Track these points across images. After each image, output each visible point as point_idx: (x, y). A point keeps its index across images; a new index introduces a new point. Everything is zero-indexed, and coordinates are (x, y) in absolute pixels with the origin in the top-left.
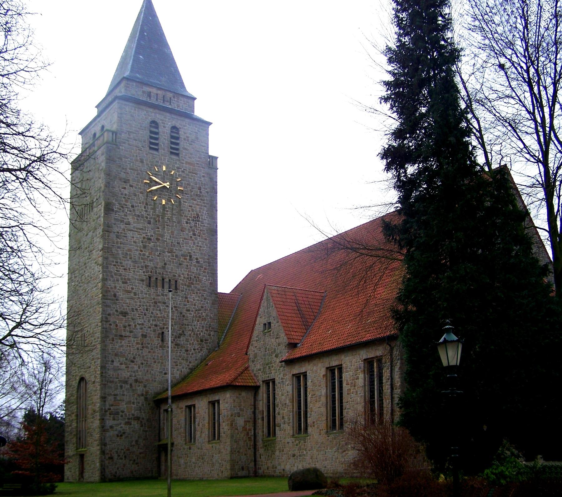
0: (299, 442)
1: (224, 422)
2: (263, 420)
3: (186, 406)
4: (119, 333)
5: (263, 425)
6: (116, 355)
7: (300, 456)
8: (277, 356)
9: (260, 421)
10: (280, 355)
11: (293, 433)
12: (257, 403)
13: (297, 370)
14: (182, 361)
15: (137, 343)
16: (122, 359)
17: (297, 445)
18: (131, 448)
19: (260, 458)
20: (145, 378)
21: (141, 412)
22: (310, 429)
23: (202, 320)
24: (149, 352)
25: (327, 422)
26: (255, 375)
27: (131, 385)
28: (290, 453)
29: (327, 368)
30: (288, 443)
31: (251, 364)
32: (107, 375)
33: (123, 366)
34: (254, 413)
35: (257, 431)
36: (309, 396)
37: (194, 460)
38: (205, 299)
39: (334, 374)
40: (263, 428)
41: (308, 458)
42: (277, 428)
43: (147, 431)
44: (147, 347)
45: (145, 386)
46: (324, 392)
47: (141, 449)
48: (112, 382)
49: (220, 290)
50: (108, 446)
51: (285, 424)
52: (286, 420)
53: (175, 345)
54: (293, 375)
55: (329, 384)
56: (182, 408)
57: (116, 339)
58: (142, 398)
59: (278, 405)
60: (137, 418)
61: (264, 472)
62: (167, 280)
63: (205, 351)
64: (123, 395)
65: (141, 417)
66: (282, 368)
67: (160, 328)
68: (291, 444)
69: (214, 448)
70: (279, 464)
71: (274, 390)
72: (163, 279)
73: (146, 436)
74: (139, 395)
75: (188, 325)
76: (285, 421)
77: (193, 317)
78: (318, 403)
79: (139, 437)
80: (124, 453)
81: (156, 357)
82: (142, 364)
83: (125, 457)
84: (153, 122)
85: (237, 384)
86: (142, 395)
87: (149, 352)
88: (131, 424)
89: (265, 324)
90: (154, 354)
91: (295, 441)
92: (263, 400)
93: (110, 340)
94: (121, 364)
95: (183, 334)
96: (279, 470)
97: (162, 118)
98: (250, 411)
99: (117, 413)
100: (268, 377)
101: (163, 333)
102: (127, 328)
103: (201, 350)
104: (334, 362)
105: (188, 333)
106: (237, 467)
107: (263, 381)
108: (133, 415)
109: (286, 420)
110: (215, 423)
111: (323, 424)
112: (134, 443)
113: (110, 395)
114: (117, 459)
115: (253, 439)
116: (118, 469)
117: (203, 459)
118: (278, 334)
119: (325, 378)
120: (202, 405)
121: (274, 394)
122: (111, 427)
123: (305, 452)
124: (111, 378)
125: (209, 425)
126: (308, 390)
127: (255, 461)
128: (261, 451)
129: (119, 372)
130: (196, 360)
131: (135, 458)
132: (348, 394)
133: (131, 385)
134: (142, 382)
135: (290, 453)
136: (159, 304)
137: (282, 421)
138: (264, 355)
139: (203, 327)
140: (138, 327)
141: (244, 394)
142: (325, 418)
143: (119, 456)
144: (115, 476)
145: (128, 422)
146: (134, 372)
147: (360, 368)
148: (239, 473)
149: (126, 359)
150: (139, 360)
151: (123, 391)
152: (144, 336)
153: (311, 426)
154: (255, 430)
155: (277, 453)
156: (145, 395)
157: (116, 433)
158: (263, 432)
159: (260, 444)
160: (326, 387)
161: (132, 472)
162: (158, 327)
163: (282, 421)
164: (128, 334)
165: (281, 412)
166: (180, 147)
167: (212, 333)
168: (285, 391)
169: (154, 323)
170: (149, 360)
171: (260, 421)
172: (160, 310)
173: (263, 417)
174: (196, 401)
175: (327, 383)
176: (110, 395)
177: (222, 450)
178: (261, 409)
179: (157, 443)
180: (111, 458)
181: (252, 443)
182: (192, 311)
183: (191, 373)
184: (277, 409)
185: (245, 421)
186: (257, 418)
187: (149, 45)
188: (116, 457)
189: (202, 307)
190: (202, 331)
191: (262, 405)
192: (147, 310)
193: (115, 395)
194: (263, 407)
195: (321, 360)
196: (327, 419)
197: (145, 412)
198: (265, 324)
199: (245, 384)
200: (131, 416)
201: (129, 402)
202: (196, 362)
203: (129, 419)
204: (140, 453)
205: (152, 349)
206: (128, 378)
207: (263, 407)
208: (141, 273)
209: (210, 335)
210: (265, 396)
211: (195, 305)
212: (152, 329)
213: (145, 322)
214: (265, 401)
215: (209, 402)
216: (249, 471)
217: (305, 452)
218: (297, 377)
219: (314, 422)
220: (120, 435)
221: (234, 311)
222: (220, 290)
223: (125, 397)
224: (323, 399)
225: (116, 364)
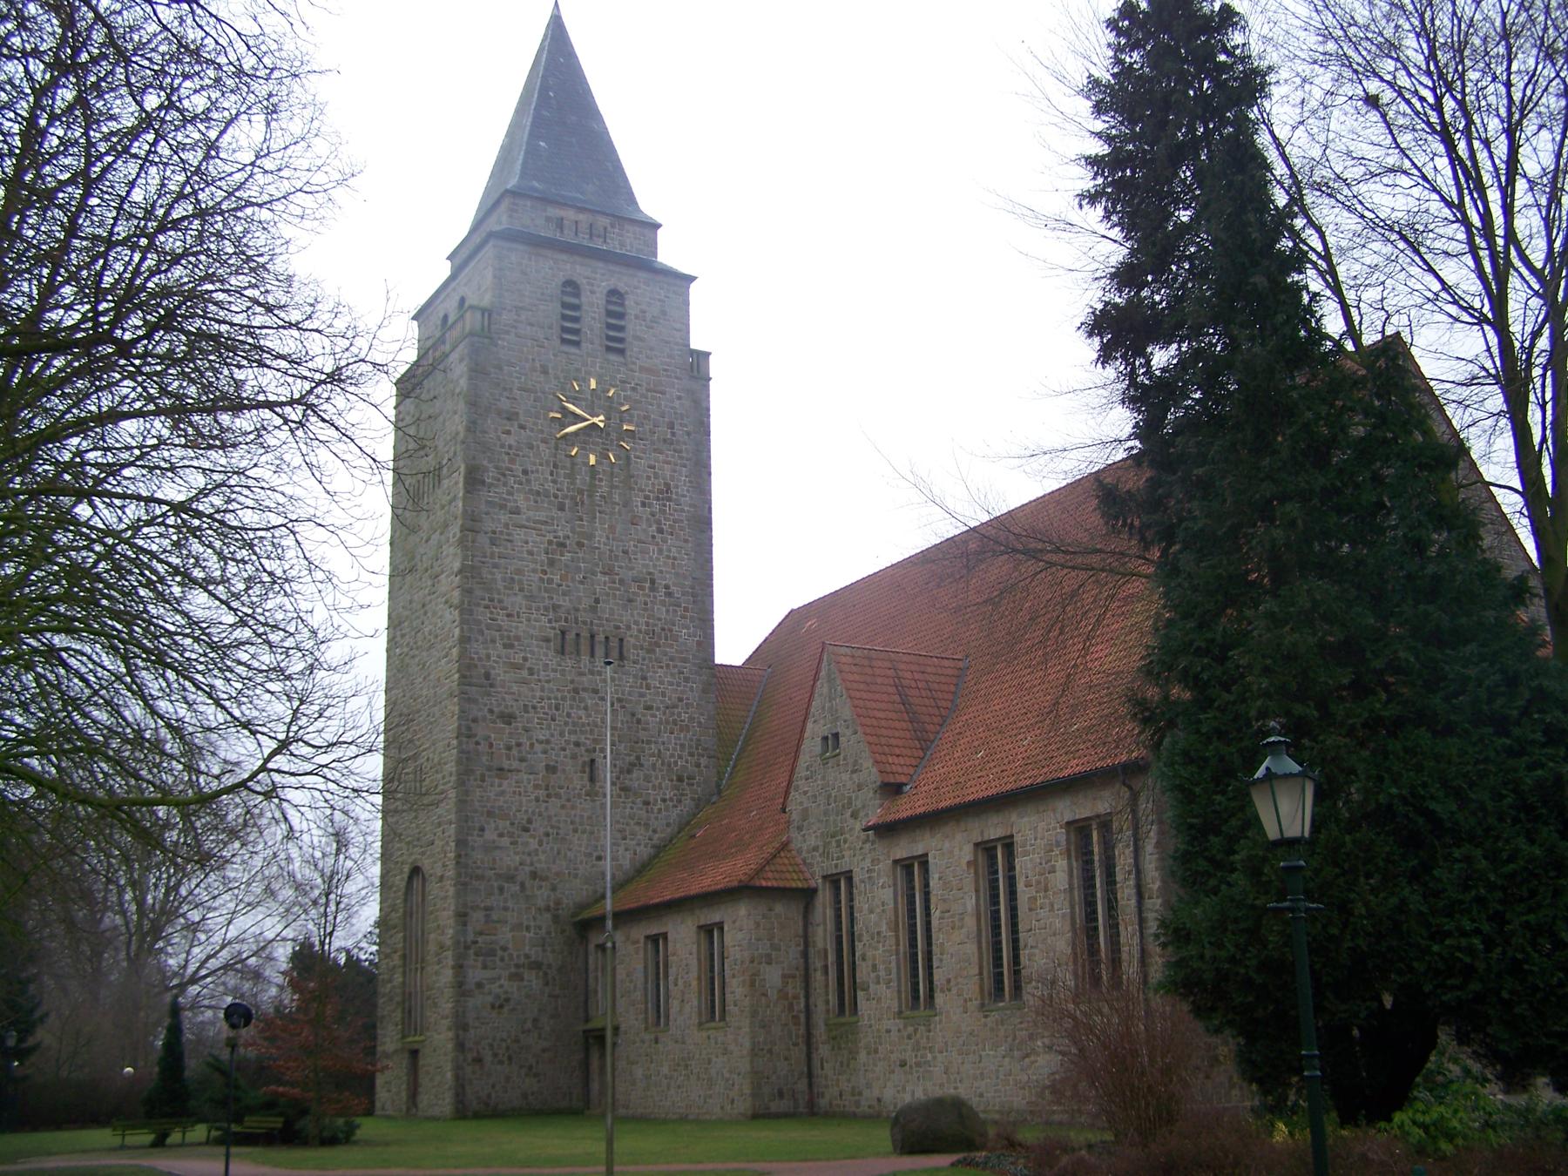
0: (916, 1031)
3: (647, 937)
6: (490, 814)
7: (918, 1064)
8: (854, 815)
13: (905, 848)
15: (536, 787)
16: (504, 825)
17: (909, 1037)
20: (555, 868)
22: (939, 999)
24: (563, 807)
27: (522, 885)
28: (894, 1057)
29: (977, 845)
30: (888, 1031)
33: (505, 841)
34: (805, 955)
35: (812, 1000)
36: (936, 915)
37: (665, 1070)
38: (687, 680)
39: (995, 859)
42: (860, 994)
43: (557, 997)
44: (558, 796)
45: (554, 889)
46: (970, 903)
54: (896, 862)
56: (638, 942)
58: (548, 916)
60: (536, 966)
64: (506, 909)
66: (868, 846)
68: (894, 1034)
70: (869, 1086)
72: (592, 637)
77: (661, 723)
80: (508, 1048)
82: (547, 835)
83: (510, 1058)
85: (764, 884)
86: (548, 909)
87: (563, 807)
89: (825, 739)
94: (501, 835)
99: (492, 953)
101: (593, 761)
102: (515, 752)
103: (680, 801)
104: (993, 828)
107: (825, 877)
108: (527, 957)
109: (882, 973)
112: (529, 1025)
113: (475, 908)
120: (682, 934)
122: (479, 985)
126: (933, 900)
127: (810, 1075)
128: (823, 1050)
130: (668, 825)
133: (522, 885)
134: (545, 879)
138: (826, 813)
140: (538, 747)
141: (779, 908)
143: (495, 1055)
144: (487, 1105)
147: (1058, 845)
150: (539, 826)
152: (551, 769)
153: (942, 991)
154: (807, 997)
157: (490, 999)
158: (827, 1002)
159: (820, 1031)
160: (977, 891)
161: (525, 1096)
164: (515, 764)
165: (869, 954)
166: (628, 335)
167: (703, 761)
168: (877, 901)
169: (573, 738)
172: (586, 708)
173: (826, 967)
175: (977, 882)
177: (732, 1047)
178: (820, 945)
179: (582, 1027)
180: (478, 1060)
181: (802, 1031)
183: (656, 856)
185: (784, 976)
189: (680, 700)
190: (680, 757)
191: (823, 937)
192: (557, 709)
193: (487, 909)
196: (981, 973)
197: (553, 951)
198: (825, 739)
199: (781, 884)
200: (522, 960)
201: (518, 927)
203: (517, 966)
204: (544, 1050)
210: (830, 913)
211: (664, 694)
214: (830, 926)
215: (700, 927)
218: (906, 865)
219: (949, 981)
220: (498, 1006)
224: (970, 922)
225: (490, 835)
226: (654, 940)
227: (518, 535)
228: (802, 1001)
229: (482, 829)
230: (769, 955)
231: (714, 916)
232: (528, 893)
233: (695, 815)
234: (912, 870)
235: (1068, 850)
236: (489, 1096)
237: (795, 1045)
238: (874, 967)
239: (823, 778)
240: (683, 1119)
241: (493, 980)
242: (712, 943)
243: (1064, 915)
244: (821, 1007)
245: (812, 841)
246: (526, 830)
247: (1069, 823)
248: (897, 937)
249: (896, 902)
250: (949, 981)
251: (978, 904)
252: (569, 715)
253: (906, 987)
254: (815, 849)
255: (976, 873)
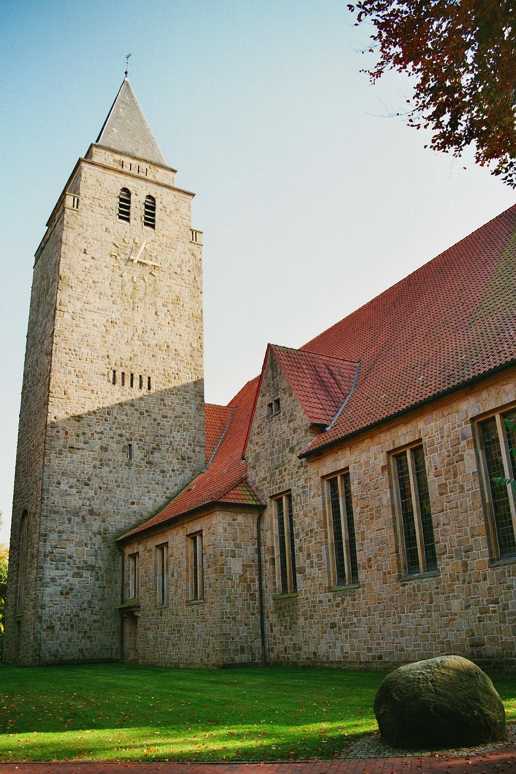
0: (343, 600)
1: (209, 567)
2: (274, 564)
3: (157, 546)
4: (69, 443)
5: (274, 572)
6: (63, 474)
7: (346, 626)
8: (292, 450)
9: (268, 566)
10: (297, 448)
11: (330, 583)
12: (262, 534)
13: (329, 465)
14: (157, 486)
15: (94, 459)
16: (73, 481)
17: (338, 605)
18: (81, 613)
19: (272, 631)
20: (104, 509)
21: (96, 559)
22: (362, 575)
23: (184, 430)
24: (111, 472)
25: (398, 556)
26: (257, 488)
27: (83, 517)
28: (325, 621)
29: (389, 453)
30: (321, 602)
31: (250, 472)
32: (49, 503)
33: (74, 491)
34: (258, 551)
35: (264, 583)
36: (356, 510)
37: (166, 634)
38: (187, 402)
39: (407, 463)
40: (274, 578)
41: (362, 630)
42: (298, 576)
43: (104, 587)
44: (108, 465)
45: (103, 521)
46: (386, 498)
47: (95, 614)
48: (56, 512)
49: (208, 400)
50: (47, 609)
51: (312, 567)
52: (315, 560)
53: (147, 463)
54: (323, 477)
55: (395, 483)
56: (151, 550)
57: (65, 451)
58: (98, 537)
59: (298, 534)
60: (91, 568)
61: (278, 656)
62: (136, 376)
63: (188, 473)
64: (72, 532)
65: (97, 566)
66: (302, 470)
67: (127, 440)
68: (326, 605)
69: (195, 613)
70: (306, 643)
71: (290, 510)
72: (132, 375)
73: (103, 595)
74: (94, 533)
75: (164, 436)
76: (312, 562)
77: (172, 425)
78: (375, 522)
79: (92, 596)
80: (71, 620)
81: (119, 480)
82: (101, 488)
83: (72, 626)
84: (125, 189)
85: (229, 501)
86: (99, 533)
87: (111, 472)
88: (82, 577)
89: (270, 405)
90: (117, 475)
91: (334, 597)
92: (271, 529)
93: (56, 453)
94: (71, 487)
95: (157, 448)
96: (305, 653)
97: (135, 185)
98: (251, 549)
99: (62, 560)
100: (279, 488)
101: (130, 445)
102: (81, 438)
103: (183, 471)
104: (403, 435)
105: (164, 448)
106: (232, 647)
107: (271, 497)
108: (85, 562)
109: (315, 560)
110: (196, 570)
111: (389, 562)
112: (85, 605)
113: (53, 530)
114: (60, 629)
115: (257, 594)
116: (60, 645)
117: (179, 631)
118: (292, 415)
119: (386, 473)
120: (177, 539)
121: (291, 517)
122: (53, 580)
123: (355, 620)
124: (56, 506)
125: (187, 574)
126: (354, 500)
127: (263, 636)
128: (272, 618)
129: (67, 498)
130: (176, 485)
131: (87, 628)
132: (441, 494)
133: (83, 517)
134: (99, 515)
135: (325, 621)
136: (125, 407)
137: (308, 562)
138: (272, 454)
139: (185, 439)
140: (96, 436)
141: (240, 518)
142: (393, 550)
143: (63, 624)
144: (56, 656)
145: (79, 573)
146: (89, 499)
147: (464, 438)
148: (236, 657)
149: (78, 481)
150: (95, 483)
151: (73, 526)
152: (104, 449)
153: (364, 568)
154: (260, 580)
155: (301, 621)
156: (103, 533)
157: (59, 588)
158: (274, 584)
159: (270, 604)
160: (391, 488)
161: (81, 651)
162: (124, 438)
163: (308, 562)
164: (81, 445)
165: (305, 546)
166: (157, 218)
167: (197, 449)
168: (312, 504)
169: (119, 431)
170: (109, 483)
171: (268, 566)
172: (126, 415)
173: (273, 559)
174: (170, 537)
175: (390, 481)
176: (53, 530)
177: (208, 617)
178: (269, 544)
179: (120, 606)
180: (51, 628)
181: (257, 604)
182: (171, 418)
183: (168, 503)
184: (296, 541)
185: (244, 566)
186: (263, 559)
187: (154, 229)
188: (58, 626)
189: (184, 413)
190: (183, 446)
191: (271, 538)
192: (109, 414)
193: (59, 532)
194: (272, 541)
195: (376, 439)
196: (397, 552)
197: (102, 560)
198: (270, 405)
199: (241, 502)
200: (82, 564)
201: (80, 544)
202: (176, 488)
203: (78, 568)
204: (95, 621)
205: (114, 468)
206: (80, 508)
207: (272, 541)
208: (101, 366)
209: (194, 451)
210: (275, 522)
211: (174, 410)
212: (115, 440)
213: (105, 430)
214: (276, 531)
215: (188, 536)
216: (253, 655)
217: (355, 620)
218: (331, 479)
219: (369, 560)
220: (65, 593)
221: (227, 426)
222: (208, 400)
223: (74, 535)
224: (387, 513)
225: (63, 487)
226: (161, 547)
227: (88, 316)
228: (257, 583)
229: (59, 483)
230: (233, 551)
231: (194, 527)
232: (88, 522)
233: (192, 480)
234: (337, 482)
235: (474, 441)
236: (57, 650)
237: (253, 614)
238: (309, 555)
239: (269, 431)
240: (177, 667)
241: (61, 577)
242: (195, 546)
243: (233, 660)
244: (270, 586)
245: (262, 475)
246: (87, 485)
247: (473, 420)
248: (326, 532)
249: (324, 507)
250: (369, 560)
251: (392, 497)
252: (116, 418)
253: (333, 568)
254: (265, 479)
255: (389, 474)
